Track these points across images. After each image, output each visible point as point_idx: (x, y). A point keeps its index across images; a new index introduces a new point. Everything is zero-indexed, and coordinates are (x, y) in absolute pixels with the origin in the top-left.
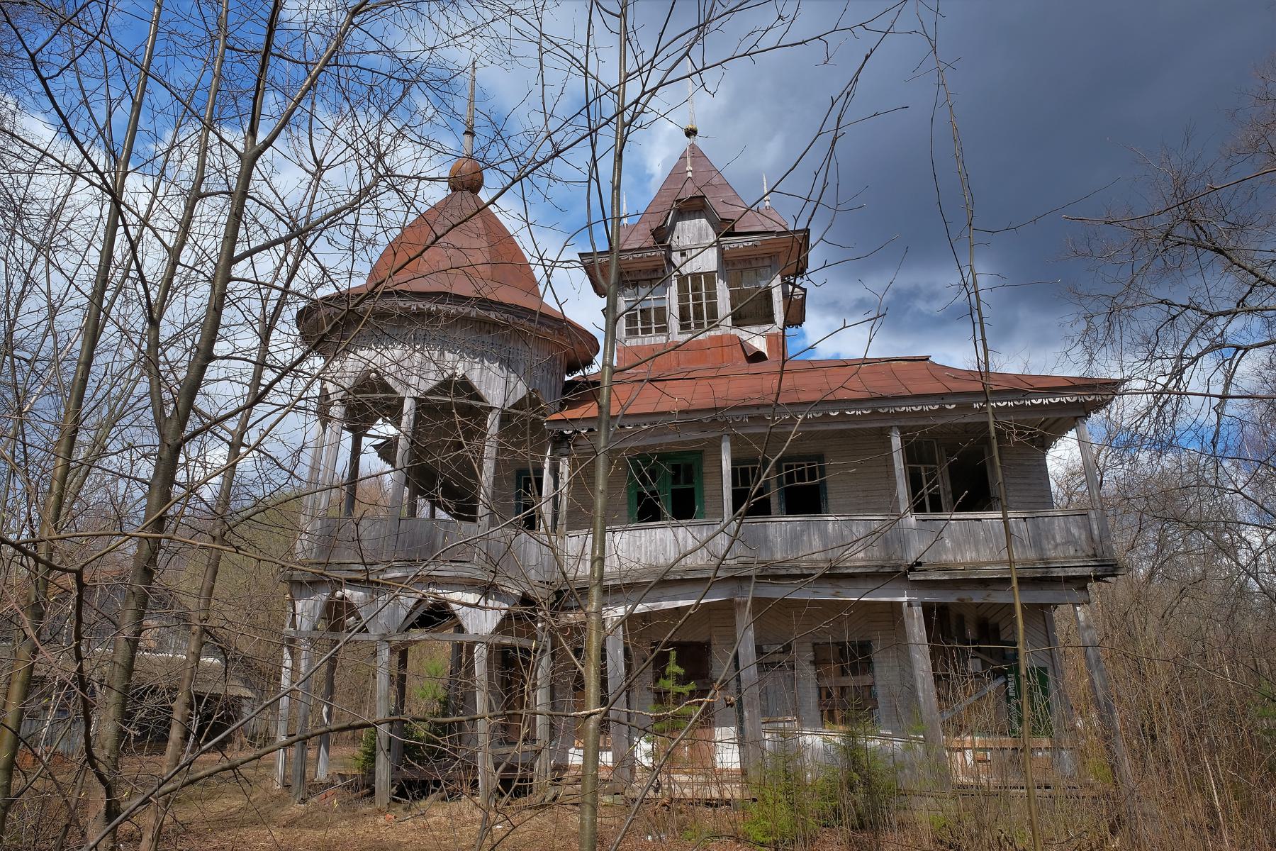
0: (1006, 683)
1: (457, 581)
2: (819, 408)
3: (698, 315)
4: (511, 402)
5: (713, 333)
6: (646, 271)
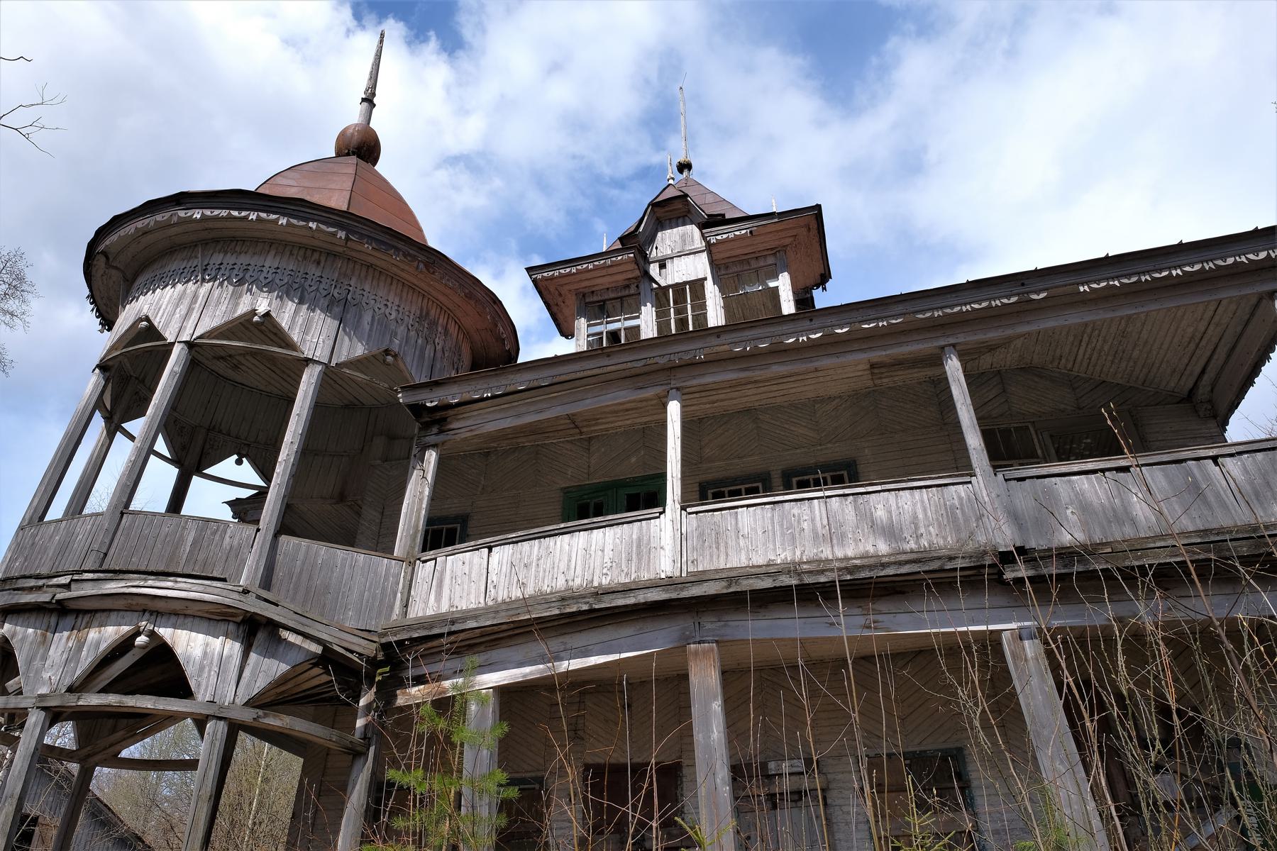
1: (194, 609)
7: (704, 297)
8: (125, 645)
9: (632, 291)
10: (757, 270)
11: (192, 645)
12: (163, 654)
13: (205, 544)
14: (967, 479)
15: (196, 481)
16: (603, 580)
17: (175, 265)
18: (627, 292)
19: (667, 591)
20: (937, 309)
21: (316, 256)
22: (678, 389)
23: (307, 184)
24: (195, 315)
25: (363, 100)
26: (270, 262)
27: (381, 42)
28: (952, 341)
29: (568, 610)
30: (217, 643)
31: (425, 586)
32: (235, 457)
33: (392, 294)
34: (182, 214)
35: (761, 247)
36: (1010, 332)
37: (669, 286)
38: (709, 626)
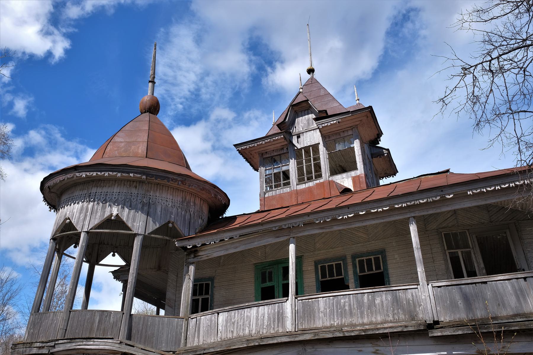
2: (351, 210)
3: (309, 172)
5: (318, 182)
6: (277, 150)
7: (319, 154)
9: (285, 152)
10: (344, 138)
13: (103, 322)
14: (416, 287)
15: (97, 267)
16: (264, 332)
17: (77, 193)
18: (282, 152)
19: (289, 338)
20: (404, 203)
21: (135, 184)
22: (294, 238)
23: (128, 140)
24: (88, 218)
26: (116, 190)
28: (413, 215)
29: (250, 345)
31: (193, 330)
32: (112, 253)
33: (169, 195)
34: (77, 174)
35: (345, 127)
36: (439, 211)
37: (302, 148)
38: (309, 350)
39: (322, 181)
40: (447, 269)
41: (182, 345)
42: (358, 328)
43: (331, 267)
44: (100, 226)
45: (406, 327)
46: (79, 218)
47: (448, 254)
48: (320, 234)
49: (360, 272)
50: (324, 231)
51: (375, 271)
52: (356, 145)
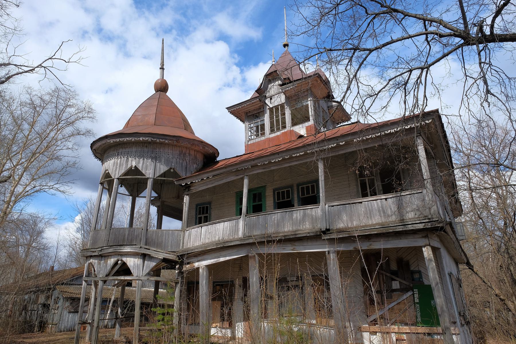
0: (413, 294)
1: (129, 253)
2: (280, 155)
4: (158, 174)
5: (283, 131)
8: (116, 264)
11: (131, 262)
12: (124, 264)
15: (137, 198)
16: (226, 238)
18: (260, 111)
21: (146, 144)
24: (118, 169)
25: (160, 68)
26: (134, 149)
27: (163, 43)
30: (136, 260)
34: (108, 141)
39: (286, 130)
40: (358, 191)
41: (181, 248)
42: (281, 235)
43: (283, 192)
44: (126, 174)
45: (309, 233)
46: (113, 169)
47: (359, 181)
48: (277, 170)
49: (302, 195)
50: (265, 170)
51: (311, 195)
52: (310, 103)
